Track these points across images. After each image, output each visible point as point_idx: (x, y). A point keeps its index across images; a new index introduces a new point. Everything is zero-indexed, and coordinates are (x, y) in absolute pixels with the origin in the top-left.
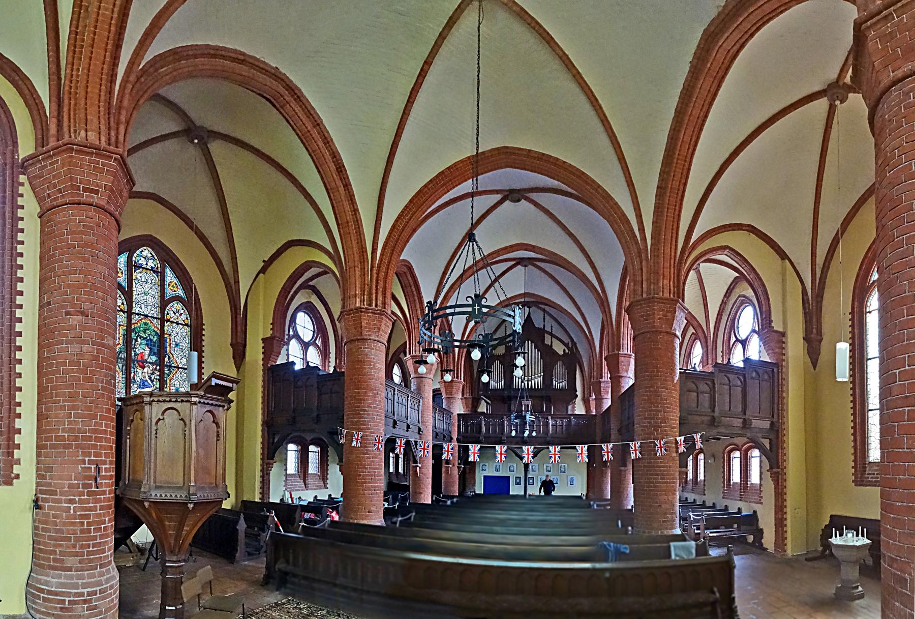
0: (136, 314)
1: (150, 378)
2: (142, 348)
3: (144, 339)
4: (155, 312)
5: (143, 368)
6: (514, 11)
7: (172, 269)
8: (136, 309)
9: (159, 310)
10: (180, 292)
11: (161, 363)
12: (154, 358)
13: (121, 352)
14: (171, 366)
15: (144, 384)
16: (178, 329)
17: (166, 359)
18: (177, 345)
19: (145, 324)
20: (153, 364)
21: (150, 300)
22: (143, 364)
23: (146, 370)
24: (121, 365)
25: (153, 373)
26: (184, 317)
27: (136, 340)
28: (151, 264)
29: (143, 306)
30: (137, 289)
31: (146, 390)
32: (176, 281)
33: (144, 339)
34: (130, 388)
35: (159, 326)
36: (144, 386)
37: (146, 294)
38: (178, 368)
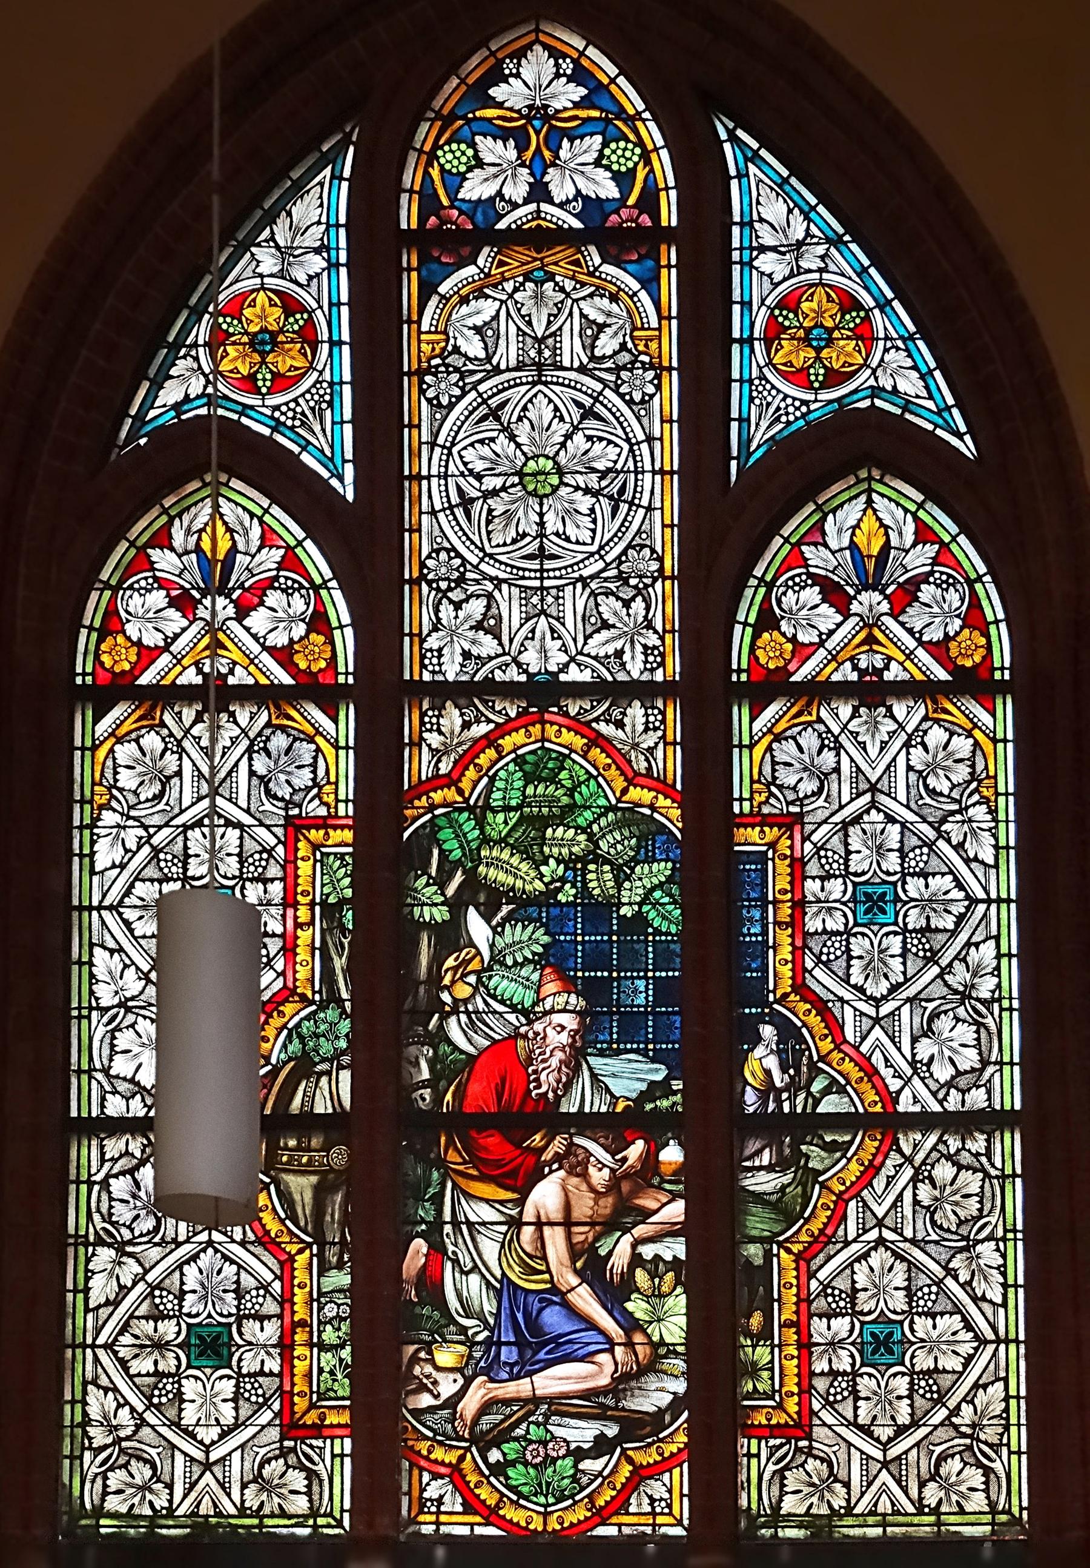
0: (443, 693)
1: (591, 1266)
2: (504, 999)
3: (526, 907)
4: (640, 637)
5: (522, 1181)
6: (220, 816)
7: (810, 165)
8: (447, 642)
9: (666, 603)
10: (905, 375)
11: (711, 1122)
12: (627, 1076)
13: (304, 1067)
14: (812, 1124)
15: (529, 1332)
16: (875, 745)
17: (763, 1060)
18: (873, 902)
19: (535, 769)
20: (615, 1127)
21: (577, 524)
22: (512, 1132)
23: (546, 1196)
24: (302, 1186)
25: (623, 1215)
26: (936, 613)
27: (451, 936)
28: (583, 175)
29: (511, 609)
30: (450, 450)
31: (555, 1380)
32: (848, 267)
33: (526, 907)
34: (404, 1381)
35: (672, 764)
36: (537, 1347)
37: (532, 482)
38: (889, 1124)
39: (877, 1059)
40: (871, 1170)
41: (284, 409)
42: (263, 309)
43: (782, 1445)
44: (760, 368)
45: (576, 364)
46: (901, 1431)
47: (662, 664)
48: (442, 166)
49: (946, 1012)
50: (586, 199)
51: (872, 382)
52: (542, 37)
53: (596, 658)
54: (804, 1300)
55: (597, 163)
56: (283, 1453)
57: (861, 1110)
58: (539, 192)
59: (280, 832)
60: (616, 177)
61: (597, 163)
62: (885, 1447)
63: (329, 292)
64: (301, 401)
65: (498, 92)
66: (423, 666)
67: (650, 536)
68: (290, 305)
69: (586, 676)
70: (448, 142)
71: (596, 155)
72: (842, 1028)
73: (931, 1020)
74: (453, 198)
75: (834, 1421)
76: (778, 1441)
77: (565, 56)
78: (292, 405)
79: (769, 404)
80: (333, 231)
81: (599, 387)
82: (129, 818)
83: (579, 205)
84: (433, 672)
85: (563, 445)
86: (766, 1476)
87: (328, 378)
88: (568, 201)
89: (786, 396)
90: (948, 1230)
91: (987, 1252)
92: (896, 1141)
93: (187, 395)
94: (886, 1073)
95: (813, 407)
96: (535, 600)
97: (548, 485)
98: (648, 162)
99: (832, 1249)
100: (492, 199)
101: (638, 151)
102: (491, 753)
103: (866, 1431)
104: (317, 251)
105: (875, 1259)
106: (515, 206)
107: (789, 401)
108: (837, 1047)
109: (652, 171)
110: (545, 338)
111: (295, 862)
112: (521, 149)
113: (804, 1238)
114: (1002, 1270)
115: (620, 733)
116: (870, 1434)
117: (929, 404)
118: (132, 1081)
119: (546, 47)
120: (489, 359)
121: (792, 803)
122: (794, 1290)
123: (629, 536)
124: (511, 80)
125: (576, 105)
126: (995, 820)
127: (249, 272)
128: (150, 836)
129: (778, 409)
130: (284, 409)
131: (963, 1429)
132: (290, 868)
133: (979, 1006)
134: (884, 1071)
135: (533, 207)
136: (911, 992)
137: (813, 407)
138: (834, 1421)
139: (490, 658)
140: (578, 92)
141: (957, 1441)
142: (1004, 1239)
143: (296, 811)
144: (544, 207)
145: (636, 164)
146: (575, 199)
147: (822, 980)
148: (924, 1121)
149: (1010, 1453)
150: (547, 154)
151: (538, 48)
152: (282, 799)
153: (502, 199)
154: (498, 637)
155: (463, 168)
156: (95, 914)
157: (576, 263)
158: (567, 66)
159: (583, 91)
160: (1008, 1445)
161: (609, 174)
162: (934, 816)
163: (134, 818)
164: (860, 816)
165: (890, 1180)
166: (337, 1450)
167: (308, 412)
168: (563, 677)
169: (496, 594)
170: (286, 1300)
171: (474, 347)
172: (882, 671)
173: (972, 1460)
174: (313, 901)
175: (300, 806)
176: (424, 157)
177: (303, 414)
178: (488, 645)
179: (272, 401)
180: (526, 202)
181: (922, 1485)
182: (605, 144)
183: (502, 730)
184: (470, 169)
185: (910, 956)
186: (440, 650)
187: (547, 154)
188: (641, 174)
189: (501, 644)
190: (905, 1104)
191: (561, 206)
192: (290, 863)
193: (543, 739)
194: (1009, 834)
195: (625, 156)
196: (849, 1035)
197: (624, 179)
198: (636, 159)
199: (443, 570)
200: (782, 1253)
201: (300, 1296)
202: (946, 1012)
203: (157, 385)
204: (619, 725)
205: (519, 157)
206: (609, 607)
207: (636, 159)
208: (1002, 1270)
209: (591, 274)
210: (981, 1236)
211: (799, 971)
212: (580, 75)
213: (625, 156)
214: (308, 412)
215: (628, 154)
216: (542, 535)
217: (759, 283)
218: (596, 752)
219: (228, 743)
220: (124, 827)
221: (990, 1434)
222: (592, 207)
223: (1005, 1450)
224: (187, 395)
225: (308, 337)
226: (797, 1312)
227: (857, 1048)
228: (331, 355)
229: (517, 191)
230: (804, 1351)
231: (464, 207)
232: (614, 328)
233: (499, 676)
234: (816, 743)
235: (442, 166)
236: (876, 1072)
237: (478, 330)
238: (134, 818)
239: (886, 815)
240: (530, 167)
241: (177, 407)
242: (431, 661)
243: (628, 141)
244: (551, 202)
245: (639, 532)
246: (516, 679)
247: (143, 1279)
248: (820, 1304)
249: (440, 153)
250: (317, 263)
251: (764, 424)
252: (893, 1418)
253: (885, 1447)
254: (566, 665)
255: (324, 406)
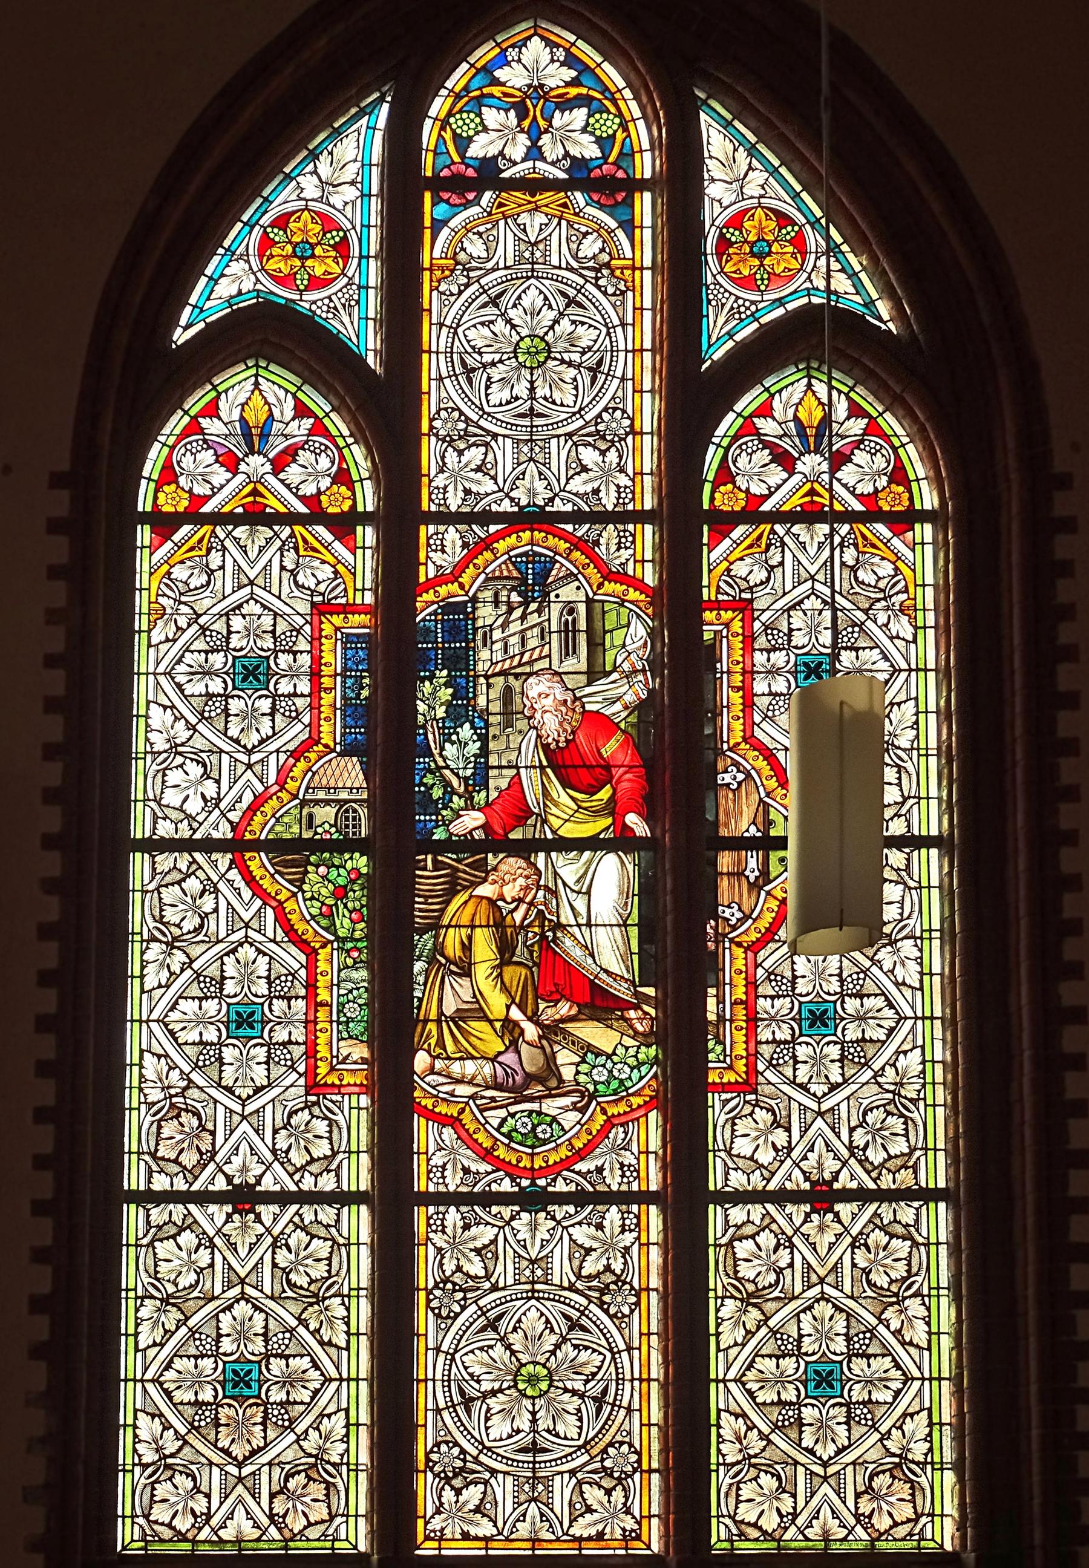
28: (575, 136)
35: (424, 1133)
38: (237, 846)
39: (247, 894)
40: (254, 808)
41: (319, 303)
42: (305, 226)
43: (336, 598)
44: (714, 276)
45: (500, 1476)
46: (834, 1087)
47: (429, 1218)
48: (454, 131)
49: (189, 932)
50: (574, 159)
51: (808, 285)
52: (540, 31)
53: (576, 495)
54: (315, 707)
55: (584, 130)
56: (307, 1106)
57: (262, 854)
58: (535, 152)
59: (761, 1079)
60: (599, 141)
61: (584, 130)
62: (252, 597)
63: (361, 213)
64: (334, 298)
65: (500, 74)
66: (638, 1217)
67: (438, 1327)
68: (327, 223)
69: (569, 508)
70: (461, 111)
71: (583, 124)
72: (276, 920)
73: (201, 926)
74: (462, 156)
75: (295, 617)
76: (339, 601)
77: (558, 46)
78: (326, 301)
79: (723, 305)
80: (366, 168)
81: (581, 281)
82: (893, 1092)
83: (567, 163)
84: (629, 1212)
85: (552, 327)
86: (720, 1123)
87: (357, 281)
88: (558, 160)
89: (738, 298)
90: (192, 760)
91: (160, 744)
92: (234, 829)
93: (240, 291)
94: (240, 883)
95: (760, 306)
96: (539, 1272)
97: (540, 356)
98: (626, 129)
99: (291, 747)
100: (495, 158)
101: (617, 120)
102: (488, 555)
103: (804, 1087)
104: (353, 183)
105: (255, 738)
106: (515, 163)
107: (740, 302)
108: (281, 903)
109: (629, 136)
110: (536, 243)
111: (748, 1054)
112: (521, 118)
113: (313, 756)
114: (920, 961)
115: (466, 1163)
116: (264, 607)
117: (858, 299)
118: (181, 809)
119: (543, 38)
120: (580, 1483)
121: (314, 1104)
122: (323, 716)
123: (454, 1329)
124: (513, 64)
125: (568, 84)
126: (141, 1090)
127: (294, 197)
128: (874, 1077)
129: (732, 308)
130: (319, 303)
131: (886, 1086)
132: (316, 643)
133: (160, 937)
134: (242, 885)
135: (530, 164)
136: (220, 947)
137: (760, 306)
138: (295, 617)
139: (580, 1223)
140: (569, 74)
141: (192, 599)
142: (146, 753)
143: (748, 1097)
144: (538, 164)
145: (615, 132)
146: (564, 158)
147: (293, 958)
148: (209, 846)
149: (926, 1105)
150: (542, 124)
151: (536, 39)
152: (309, 589)
153: (504, 158)
154: (494, 478)
155: (471, 133)
156: (920, 1014)
157: (565, 205)
158: (560, 54)
159: (574, 73)
160: (925, 1099)
161: (593, 139)
162: (193, 1093)
163: (888, 1091)
164: (256, 1092)
165: (240, 800)
166: (354, 1104)
167: (339, 307)
168: (517, 1208)
169: (573, 1279)
170: (311, 986)
171: (594, 1495)
172: (234, 1212)
173: (180, 585)
174: (731, 1021)
175: (745, 1102)
176: (439, 123)
177: (335, 308)
178: (582, 1234)
179: (310, 296)
180: (524, 160)
181: (852, 1130)
182: (590, 116)
183: (566, 1164)
184: (477, 133)
185: (218, 978)
186: (623, 1232)
187: (542, 124)
188: (620, 135)
189: (570, 1235)
190: (224, 860)
191: (553, 164)
192: (752, 1057)
193: (532, 1155)
194: (132, 1077)
195: (608, 124)
196: (270, 913)
197: (604, 142)
198: (615, 127)
199: (619, 1299)
200: (332, 745)
201: (322, 981)
202: (189, 932)
203: (214, 280)
204: (466, 1171)
205: (519, 125)
206: (589, 456)
207: (615, 127)
208: (148, 728)
209: (576, 214)
210: (165, 755)
211: (311, 966)
212: (571, 60)
213: (608, 124)
214: (339, 307)
215: (609, 123)
216: (533, 398)
217: (719, 196)
218: (577, 554)
219: (809, 1155)
220: (895, 1084)
221: (910, 1092)
222: (579, 163)
223: (921, 1103)
224: (240, 291)
225: (342, 249)
226: (746, 993)
227: (265, 903)
228: (359, 265)
229: (518, 148)
230: (752, 1023)
231: (471, 162)
232: (466, 1509)
233: (571, 1209)
234: (292, 1154)
235: (454, 131)
236: (248, 884)
237: (590, 1510)
238: (888, 1091)
239: (233, 1093)
240: (528, 133)
241: (229, 300)
242: (631, 1221)
243: (609, 113)
244: (544, 160)
245: (613, 398)
246: (556, 1207)
247: (190, 966)
248: (301, 703)
249: (452, 120)
250: (351, 193)
251: (721, 320)
252: (826, 1077)
253: (252, 597)
254: (513, 1218)
255: (353, 303)
